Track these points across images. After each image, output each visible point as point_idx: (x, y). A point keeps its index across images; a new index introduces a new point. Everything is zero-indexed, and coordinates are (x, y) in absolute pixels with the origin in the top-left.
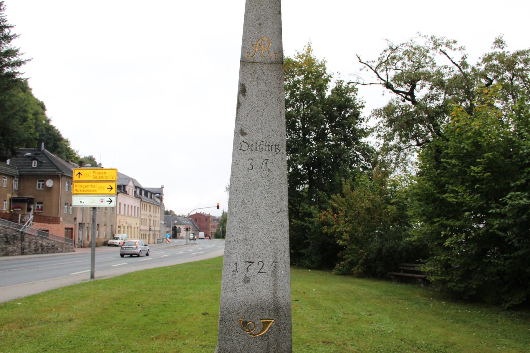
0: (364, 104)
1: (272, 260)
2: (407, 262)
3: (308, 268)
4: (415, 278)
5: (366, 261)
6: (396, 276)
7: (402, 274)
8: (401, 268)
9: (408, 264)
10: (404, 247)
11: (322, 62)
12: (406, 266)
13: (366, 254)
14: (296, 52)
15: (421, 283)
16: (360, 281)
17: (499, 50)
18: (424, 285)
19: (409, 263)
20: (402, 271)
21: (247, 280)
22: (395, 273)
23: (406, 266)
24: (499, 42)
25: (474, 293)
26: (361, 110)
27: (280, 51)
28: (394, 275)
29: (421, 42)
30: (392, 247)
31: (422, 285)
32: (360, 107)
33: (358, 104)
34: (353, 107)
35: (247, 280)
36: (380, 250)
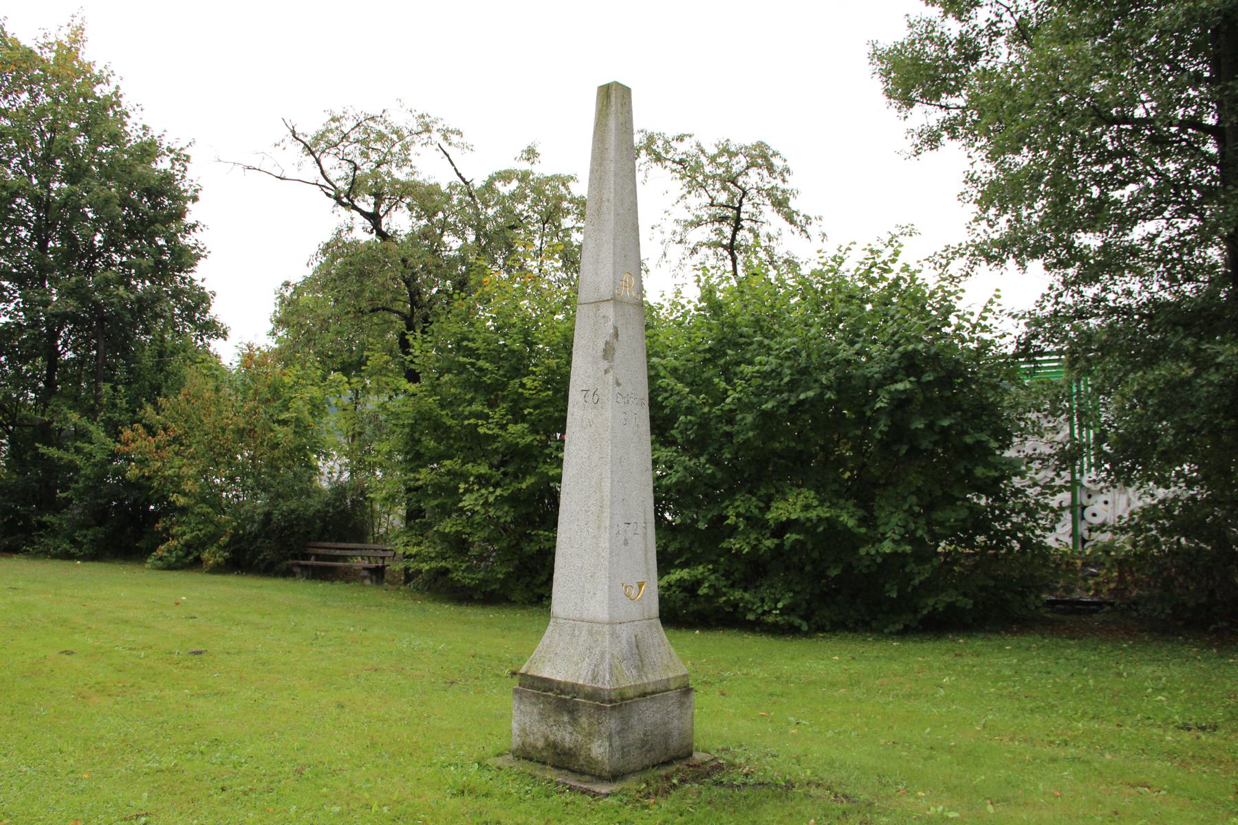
0: (200, 194)
1: (642, 521)
2: (319, 539)
3: (67, 556)
4: (334, 569)
5: (236, 539)
6: (306, 567)
7: (312, 562)
8: (311, 551)
9: (327, 544)
10: (319, 511)
11: (101, 71)
12: (326, 548)
13: (235, 524)
14: (42, 33)
15: (365, 577)
16: (218, 578)
17: (524, 166)
18: (372, 581)
19: (325, 541)
20: (313, 558)
21: (626, 543)
22: (303, 562)
23: (326, 548)
24: (531, 154)
25: (497, 586)
26: (189, 205)
27: (641, 290)
28: (300, 566)
29: (401, 119)
30: (293, 511)
31: (368, 582)
32: (189, 198)
33: (186, 191)
34: (178, 197)
35: (626, 543)
36: (268, 515)
